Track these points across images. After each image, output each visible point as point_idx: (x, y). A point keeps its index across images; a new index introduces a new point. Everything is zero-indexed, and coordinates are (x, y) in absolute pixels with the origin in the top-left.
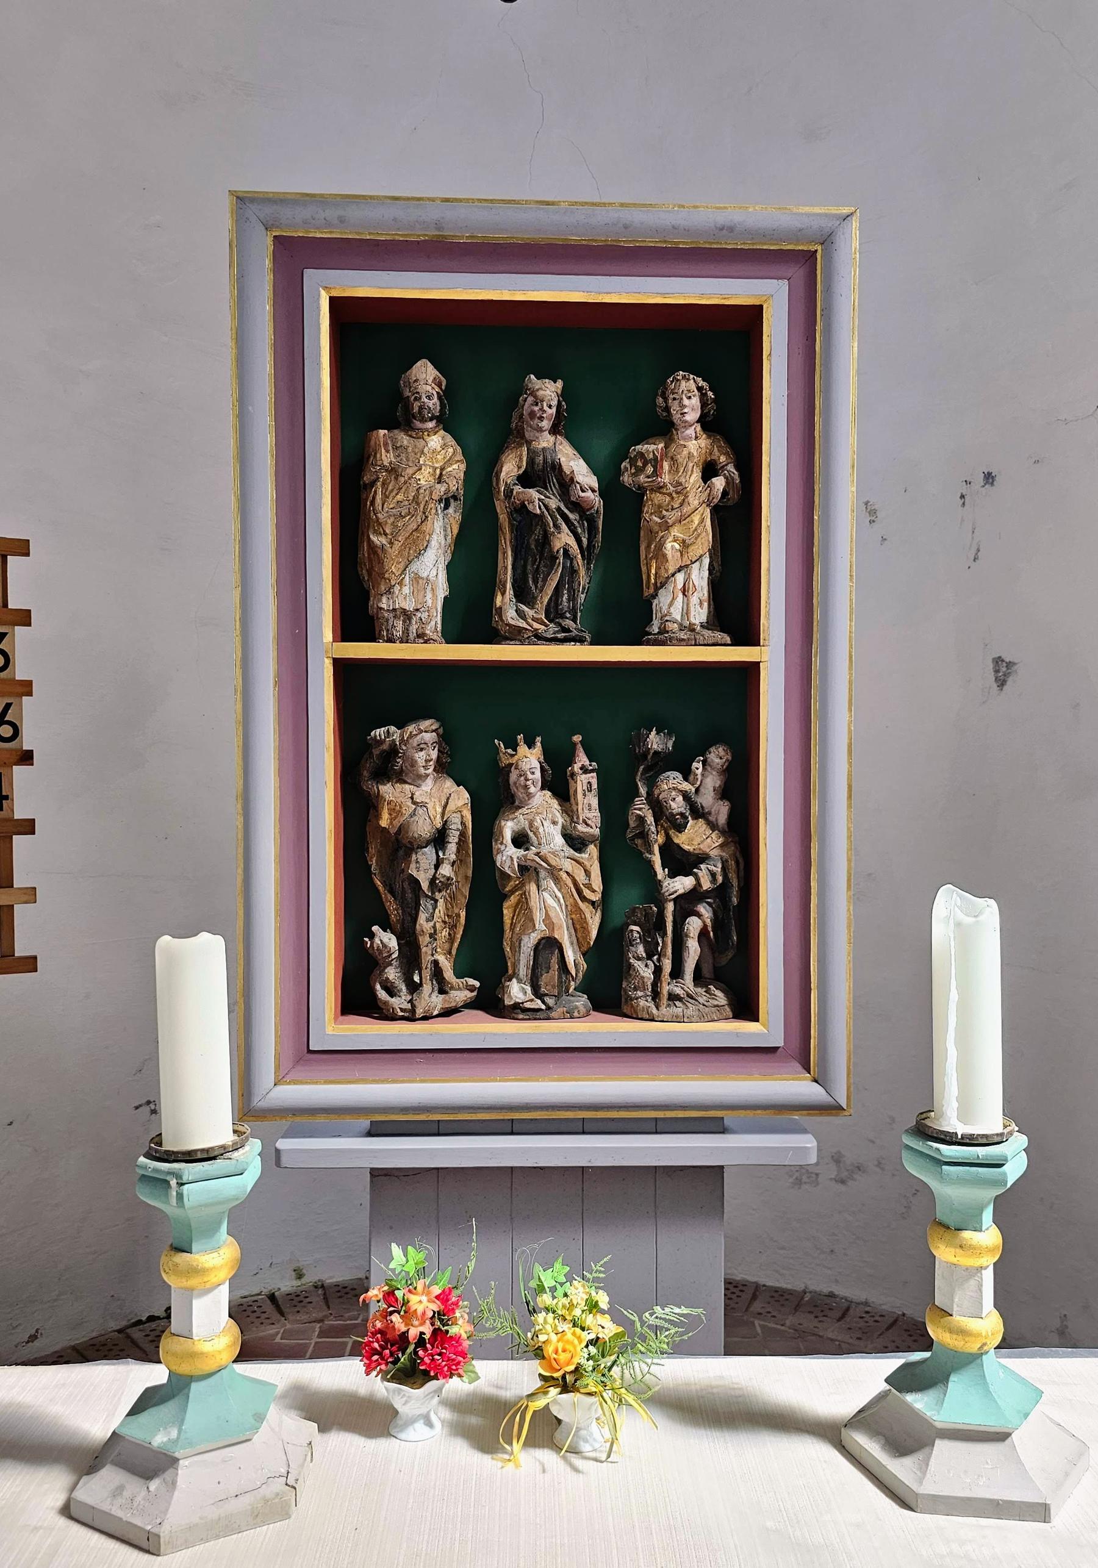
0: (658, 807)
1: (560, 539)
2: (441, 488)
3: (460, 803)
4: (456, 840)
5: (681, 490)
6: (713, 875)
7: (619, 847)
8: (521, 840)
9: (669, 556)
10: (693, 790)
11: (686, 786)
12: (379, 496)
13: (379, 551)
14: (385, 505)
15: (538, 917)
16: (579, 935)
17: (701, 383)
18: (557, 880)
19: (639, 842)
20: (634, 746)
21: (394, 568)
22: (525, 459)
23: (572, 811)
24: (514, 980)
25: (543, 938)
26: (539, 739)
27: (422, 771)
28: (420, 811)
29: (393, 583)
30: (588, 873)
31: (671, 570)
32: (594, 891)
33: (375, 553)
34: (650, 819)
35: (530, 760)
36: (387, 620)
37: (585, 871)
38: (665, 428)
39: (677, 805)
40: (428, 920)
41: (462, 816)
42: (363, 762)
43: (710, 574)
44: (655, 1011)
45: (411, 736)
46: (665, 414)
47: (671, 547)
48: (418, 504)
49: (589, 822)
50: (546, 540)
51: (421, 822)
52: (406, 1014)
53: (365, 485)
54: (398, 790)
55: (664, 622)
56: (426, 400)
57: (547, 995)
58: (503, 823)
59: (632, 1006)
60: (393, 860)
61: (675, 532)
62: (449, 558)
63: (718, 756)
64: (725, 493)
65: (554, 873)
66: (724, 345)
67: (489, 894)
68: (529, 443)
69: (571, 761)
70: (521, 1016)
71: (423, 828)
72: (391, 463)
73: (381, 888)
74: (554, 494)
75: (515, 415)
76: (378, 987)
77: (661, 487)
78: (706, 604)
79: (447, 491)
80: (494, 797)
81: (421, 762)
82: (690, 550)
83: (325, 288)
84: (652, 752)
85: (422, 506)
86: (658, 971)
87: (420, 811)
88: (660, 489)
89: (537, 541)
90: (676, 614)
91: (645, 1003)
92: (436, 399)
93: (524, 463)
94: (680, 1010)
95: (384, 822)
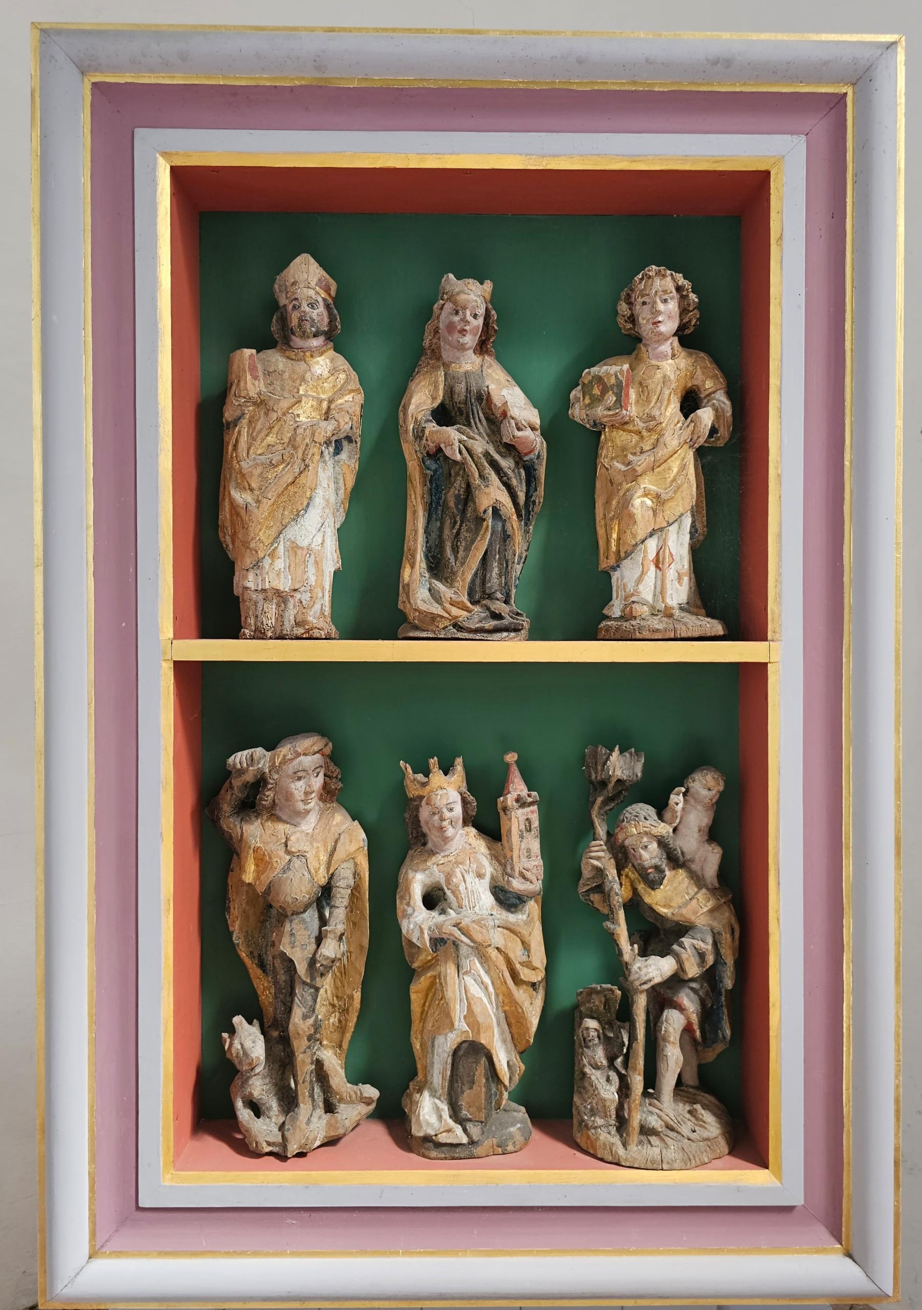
0: (622, 856)
1: (488, 494)
2: (330, 427)
3: (353, 848)
4: (346, 902)
5: (653, 425)
6: (702, 956)
7: (567, 905)
8: (432, 900)
9: (638, 517)
10: (671, 830)
11: (664, 829)
12: (244, 439)
13: (243, 512)
14: (250, 450)
15: (458, 1011)
16: (514, 1030)
17: (681, 281)
18: (484, 959)
19: (595, 898)
20: (588, 767)
21: (261, 534)
22: (441, 387)
23: (505, 857)
24: (426, 1094)
25: (464, 1042)
26: (459, 761)
27: (301, 806)
28: (297, 863)
29: (261, 555)
30: (526, 946)
31: (641, 535)
32: (534, 969)
33: (238, 514)
34: (612, 872)
35: (447, 792)
36: (256, 603)
37: (523, 943)
38: (629, 344)
39: (650, 855)
40: (305, 1017)
41: (356, 865)
42: (223, 792)
43: (691, 538)
44: (621, 1151)
45: (284, 761)
46: (629, 326)
47: (640, 504)
48: (295, 448)
49: (528, 874)
50: (468, 496)
51: (296, 882)
52: (276, 1149)
53: (228, 423)
54: (269, 832)
55: (629, 604)
56: (307, 309)
57: (470, 1120)
58: (411, 875)
59: (588, 1137)
60: (264, 921)
61: (647, 483)
62: (341, 518)
63: (706, 785)
64: (713, 431)
65: (480, 950)
66: (711, 232)
67: (392, 973)
68: (446, 366)
69: (502, 789)
70: (434, 1154)
71: (299, 887)
72: (259, 394)
73: (248, 961)
74: (480, 434)
75: (429, 328)
76: (239, 1104)
77: (626, 423)
78: (686, 579)
79: (337, 429)
80: (397, 837)
81: (298, 795)
82: (667, 506)
83: (165, 154)
84: (614, 780)
85: (300, 452)
86: (624, 1089)
87: (297, 863)
88: (624, 424)
89: (457, 497)
90: (647, 592)
91: (607, 1136)
92: (321, 308)
93: (441, 393)
94: (657, 1151)
95: (249, 876)
